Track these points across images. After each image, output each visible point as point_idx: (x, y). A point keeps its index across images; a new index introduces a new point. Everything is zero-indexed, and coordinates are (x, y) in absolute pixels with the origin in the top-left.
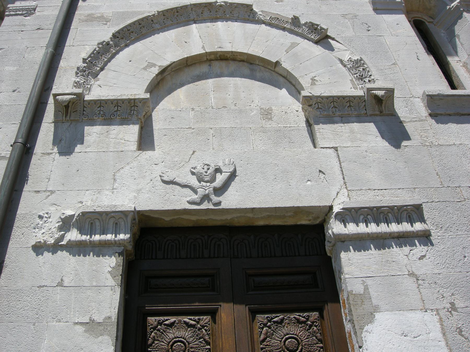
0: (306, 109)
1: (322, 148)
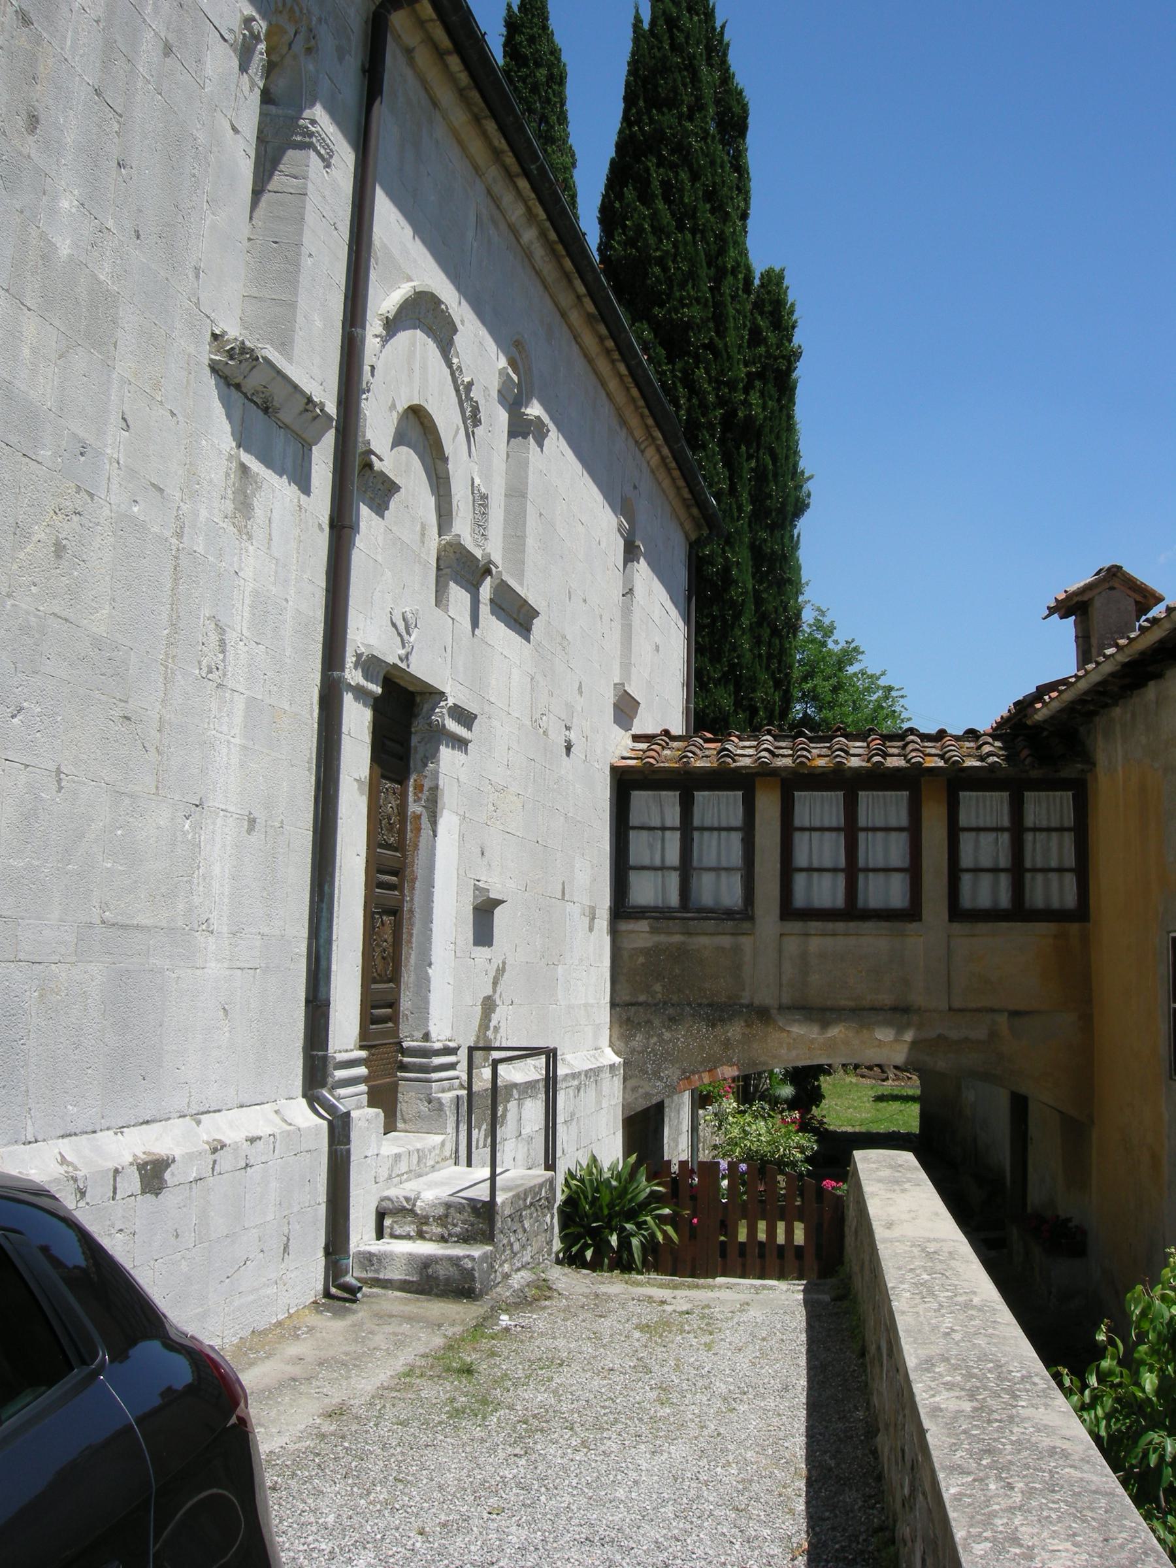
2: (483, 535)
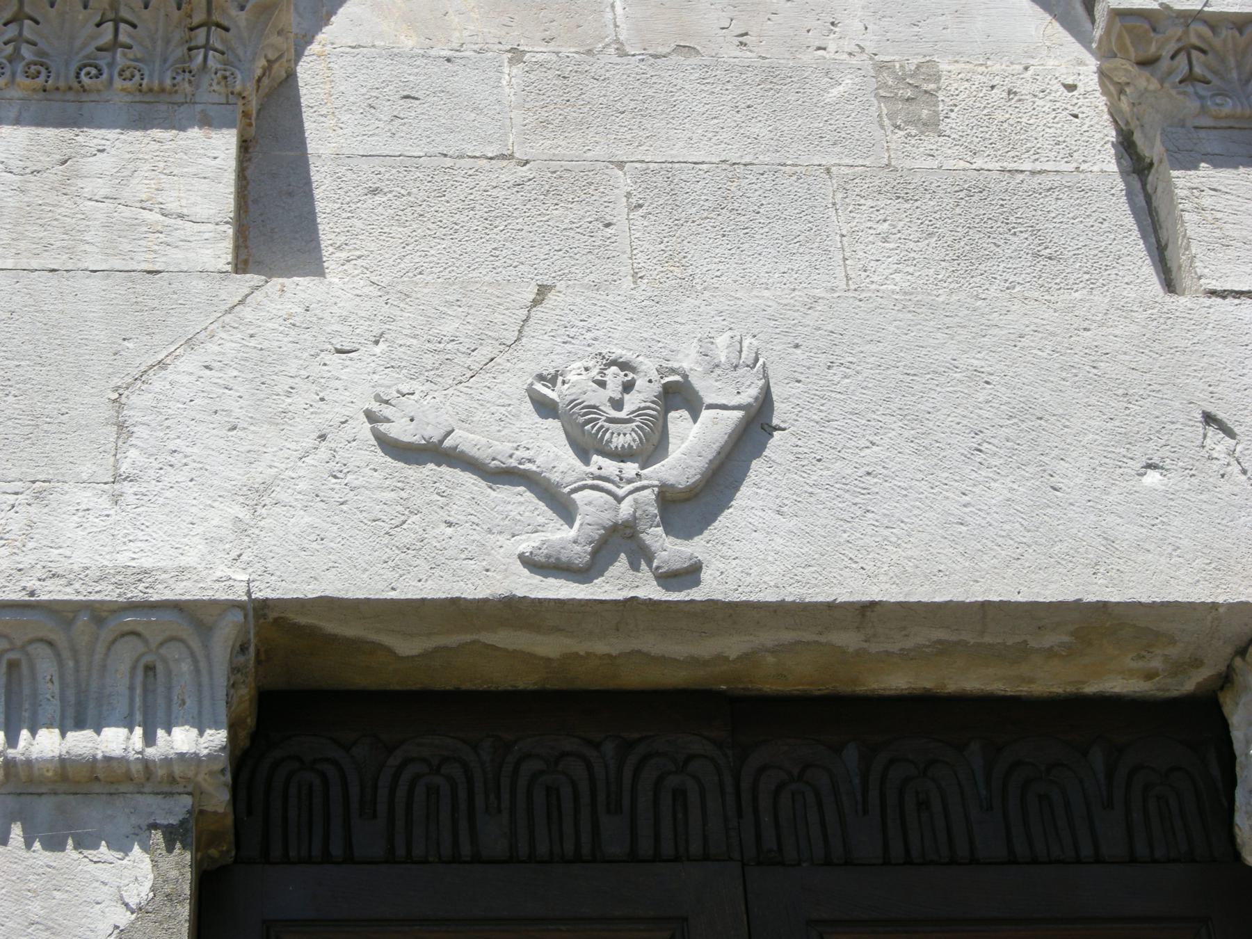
0: (1123, 79)
1: (1213, 293)
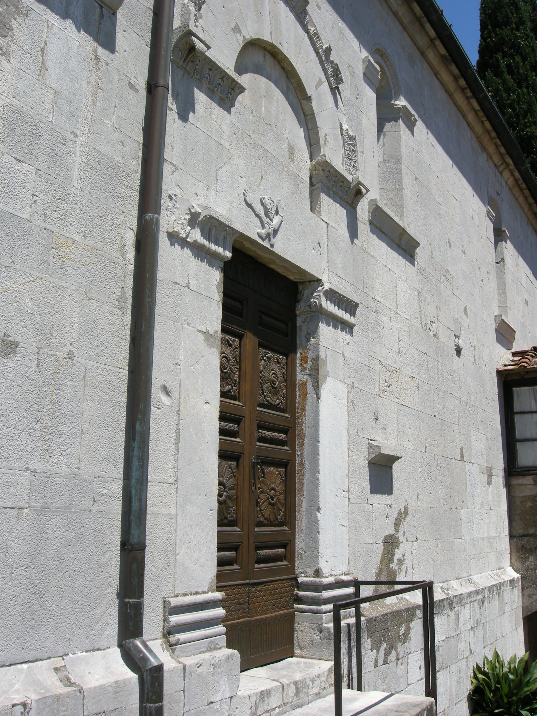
1: (322, 219)
2: (354, 166)
